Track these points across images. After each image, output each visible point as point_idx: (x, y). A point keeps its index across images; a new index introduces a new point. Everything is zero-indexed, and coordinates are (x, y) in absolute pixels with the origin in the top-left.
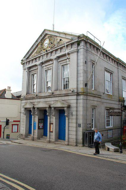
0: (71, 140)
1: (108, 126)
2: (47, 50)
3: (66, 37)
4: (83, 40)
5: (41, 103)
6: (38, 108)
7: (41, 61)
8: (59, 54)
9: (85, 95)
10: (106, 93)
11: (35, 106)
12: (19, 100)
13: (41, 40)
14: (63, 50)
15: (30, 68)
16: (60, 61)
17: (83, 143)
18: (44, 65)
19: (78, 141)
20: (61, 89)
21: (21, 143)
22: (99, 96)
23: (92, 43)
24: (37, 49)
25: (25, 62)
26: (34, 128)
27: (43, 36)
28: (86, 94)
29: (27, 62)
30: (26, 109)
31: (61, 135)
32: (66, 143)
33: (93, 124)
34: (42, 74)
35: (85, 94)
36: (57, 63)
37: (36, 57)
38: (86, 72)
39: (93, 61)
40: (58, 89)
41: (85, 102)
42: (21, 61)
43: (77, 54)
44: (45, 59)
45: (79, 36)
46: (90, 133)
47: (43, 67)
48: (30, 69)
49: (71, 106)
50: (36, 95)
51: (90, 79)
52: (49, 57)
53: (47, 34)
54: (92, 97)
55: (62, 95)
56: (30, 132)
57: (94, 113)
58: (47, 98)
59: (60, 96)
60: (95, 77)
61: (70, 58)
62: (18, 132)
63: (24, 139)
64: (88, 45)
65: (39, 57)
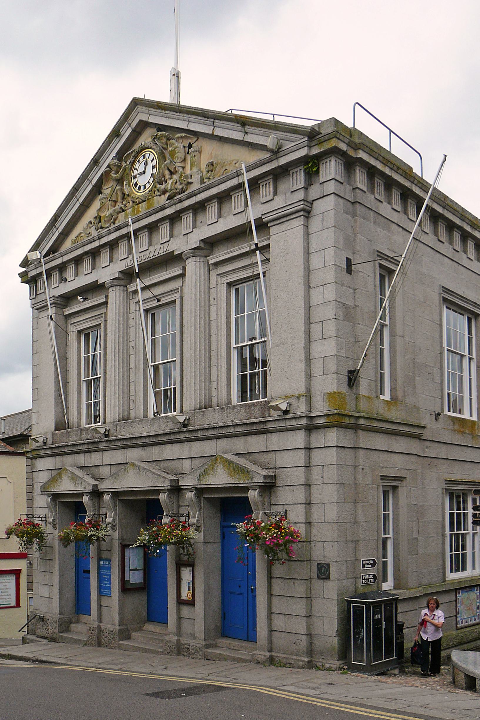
0: (279, 640)
1: (457, 570)
2: (167, 196)
3: (249, 138)
4: (335, 151)
5: (130, 468)
6: (115, 494)
7: (122, 266)
8: (214, 224)
9: (346, 427)
10: (446, 412)
11: (103, 486)
12: (23, 454)
13: (120, 155)
14: (237, 202)
15: (67, 299)
16: (217, 264)
17: (344, 654)
18: (138, 284)
19: (318, 644)
20: (229, 403)
21: (44, 658)
22: (414, 432)
23: (379, 166)
24: (96, 205)
25: (43, 269)
26: (100, 587)
27: (127, 133)
28: (353, 421)
29: (49, 273)
30: (55, 497)
31: (234, 620)
32: (263, 655)
33: (385, 564)
34: (128, 328)
35: (347, 420)
36: (203, 271)
37: (96, 244)
38: (347, 313)
39: (387, 258)
40: (214, 401)
41: (350, 462)
42: (22, 265)
43: (306, 226)
44: (141, 251)
45: (312, 128)
46: (376, 605)
47: (135, 292)
48: (65, 306)
49: (279, 483)
50: (102, 431)
51: (372, 349)
52: (165, 243)
53: (144, 125)
54: (382, 435)
55: (232, 430)
56: (81, 605)
57: (391, 512)
58: (159, 444)
59: (220, 433)
60: (392, 335)
61: (268, 246)
62: (18, 605)
63: (52, 640)
64: (360, 178)
65: (113, 245)
